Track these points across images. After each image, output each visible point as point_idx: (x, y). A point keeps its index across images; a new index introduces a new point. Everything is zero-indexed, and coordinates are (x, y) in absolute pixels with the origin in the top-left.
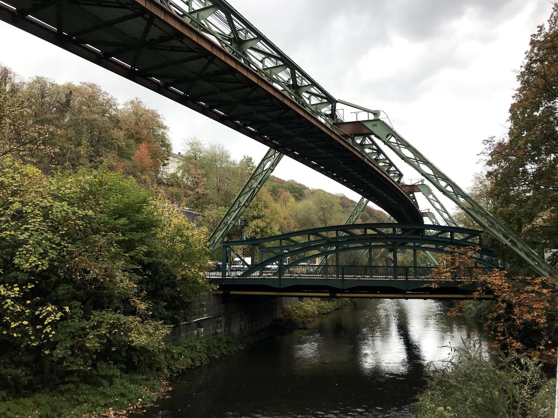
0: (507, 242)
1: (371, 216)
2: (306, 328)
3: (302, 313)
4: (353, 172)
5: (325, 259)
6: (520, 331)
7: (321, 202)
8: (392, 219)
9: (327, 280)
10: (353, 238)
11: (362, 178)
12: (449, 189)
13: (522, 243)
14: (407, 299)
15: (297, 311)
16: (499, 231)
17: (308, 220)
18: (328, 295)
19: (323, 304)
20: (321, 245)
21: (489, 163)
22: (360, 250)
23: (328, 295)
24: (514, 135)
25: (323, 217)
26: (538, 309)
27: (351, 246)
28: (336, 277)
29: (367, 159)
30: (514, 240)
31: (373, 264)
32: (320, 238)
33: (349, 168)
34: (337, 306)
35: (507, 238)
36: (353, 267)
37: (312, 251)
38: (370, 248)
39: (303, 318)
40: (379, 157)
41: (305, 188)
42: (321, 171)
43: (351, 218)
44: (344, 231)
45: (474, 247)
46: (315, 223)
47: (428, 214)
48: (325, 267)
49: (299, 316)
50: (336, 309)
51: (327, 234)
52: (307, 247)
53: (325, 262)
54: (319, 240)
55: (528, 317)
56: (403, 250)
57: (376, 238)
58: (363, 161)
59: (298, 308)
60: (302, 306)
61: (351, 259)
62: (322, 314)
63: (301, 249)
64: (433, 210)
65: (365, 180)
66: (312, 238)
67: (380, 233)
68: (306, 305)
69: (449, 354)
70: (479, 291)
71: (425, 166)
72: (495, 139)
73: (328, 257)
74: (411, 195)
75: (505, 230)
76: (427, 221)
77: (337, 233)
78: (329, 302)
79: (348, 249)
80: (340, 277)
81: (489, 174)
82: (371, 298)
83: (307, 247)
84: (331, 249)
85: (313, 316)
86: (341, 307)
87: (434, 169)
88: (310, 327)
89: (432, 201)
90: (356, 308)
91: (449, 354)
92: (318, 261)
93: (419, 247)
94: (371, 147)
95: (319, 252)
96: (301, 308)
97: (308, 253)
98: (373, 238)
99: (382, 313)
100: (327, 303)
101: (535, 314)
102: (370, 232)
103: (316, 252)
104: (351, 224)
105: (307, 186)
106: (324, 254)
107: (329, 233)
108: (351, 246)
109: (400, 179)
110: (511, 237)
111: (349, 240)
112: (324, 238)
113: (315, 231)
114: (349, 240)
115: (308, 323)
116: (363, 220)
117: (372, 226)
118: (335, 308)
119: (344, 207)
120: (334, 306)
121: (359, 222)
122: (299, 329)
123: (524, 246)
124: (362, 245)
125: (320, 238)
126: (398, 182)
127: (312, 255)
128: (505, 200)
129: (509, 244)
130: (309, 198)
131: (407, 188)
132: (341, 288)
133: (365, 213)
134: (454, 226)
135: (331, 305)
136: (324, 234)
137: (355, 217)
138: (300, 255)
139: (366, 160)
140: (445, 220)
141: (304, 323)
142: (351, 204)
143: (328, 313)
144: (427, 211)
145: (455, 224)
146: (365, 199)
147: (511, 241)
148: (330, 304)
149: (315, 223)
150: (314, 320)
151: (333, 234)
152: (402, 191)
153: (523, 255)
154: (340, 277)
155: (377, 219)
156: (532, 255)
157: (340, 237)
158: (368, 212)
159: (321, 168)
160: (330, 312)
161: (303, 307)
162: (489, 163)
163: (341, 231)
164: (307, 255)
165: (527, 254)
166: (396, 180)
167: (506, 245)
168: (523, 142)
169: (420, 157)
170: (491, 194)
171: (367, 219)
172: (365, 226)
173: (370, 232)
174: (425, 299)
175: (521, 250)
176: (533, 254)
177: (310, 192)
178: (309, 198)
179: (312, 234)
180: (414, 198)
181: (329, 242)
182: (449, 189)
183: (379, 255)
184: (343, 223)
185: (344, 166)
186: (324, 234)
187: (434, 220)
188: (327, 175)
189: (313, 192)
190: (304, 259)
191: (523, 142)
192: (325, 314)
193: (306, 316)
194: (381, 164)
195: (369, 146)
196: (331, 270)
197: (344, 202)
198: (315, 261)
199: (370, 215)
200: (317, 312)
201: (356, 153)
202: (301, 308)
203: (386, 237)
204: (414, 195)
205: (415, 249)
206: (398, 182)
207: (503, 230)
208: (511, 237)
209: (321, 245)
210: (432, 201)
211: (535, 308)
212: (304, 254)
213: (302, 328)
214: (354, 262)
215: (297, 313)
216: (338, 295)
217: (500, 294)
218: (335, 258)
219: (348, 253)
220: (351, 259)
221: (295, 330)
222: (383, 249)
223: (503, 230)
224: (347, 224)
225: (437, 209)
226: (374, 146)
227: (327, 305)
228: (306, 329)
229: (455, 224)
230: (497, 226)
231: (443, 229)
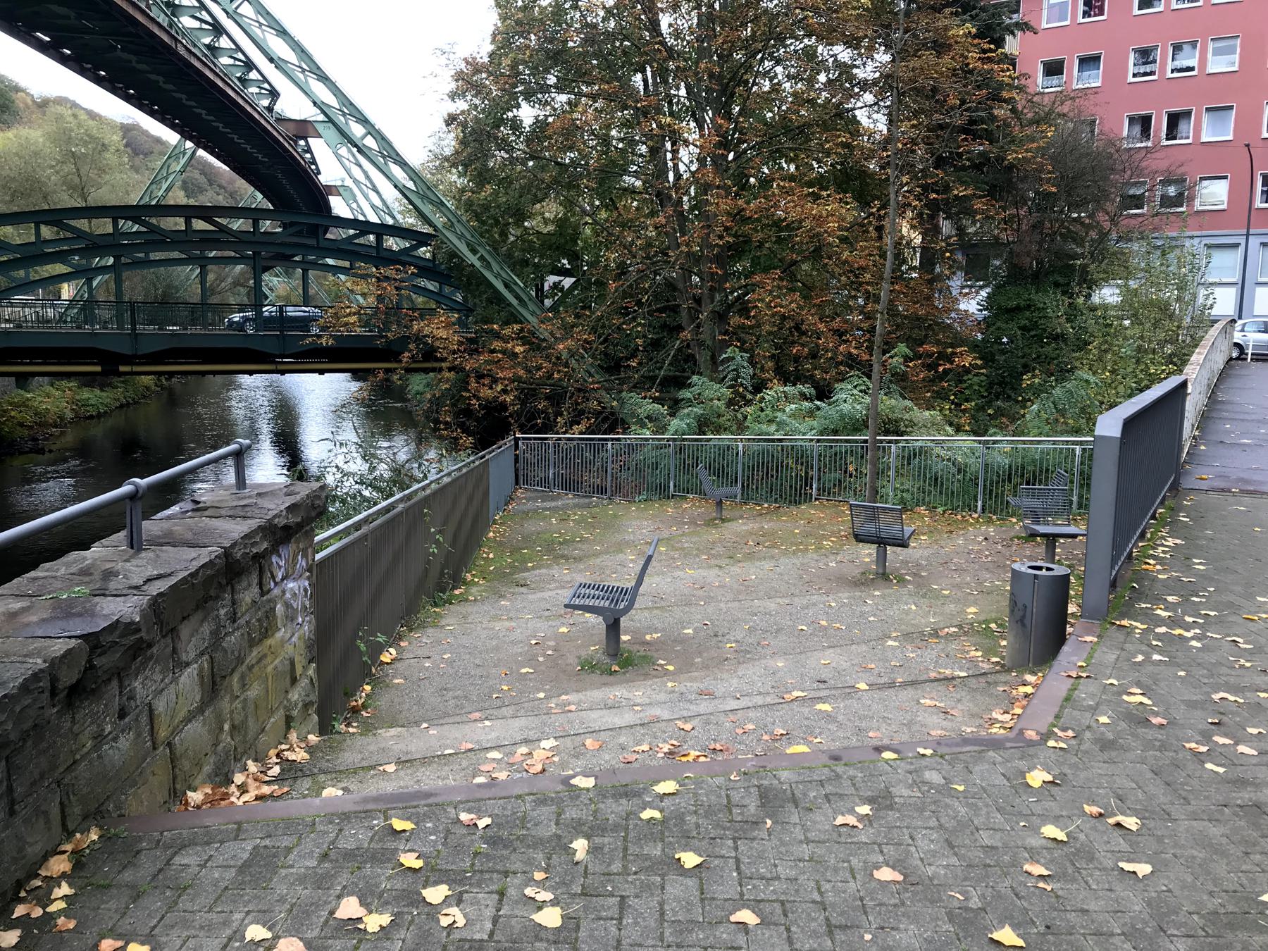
0: (472, 259)
1: (211, 182)
2: (43, 449)
3: (28, 418)
4: (150, 73)
5: (85, 288)
6: (478, 420)
7: (64, 137)
8: (259, 196)
9: (93, 335)
10: (159, 239)
11: (174, 91)
12: (370, 142)
13: (499, 263)
14: (283, 373)
15: (13, 413)
16: (461, 237)
17: (31, 184)
18: (98, 369)
19: (86, 394)
20: (73, 252)
21: (453, 96)
22: (180, 268)
23: (98, 369)
24: (503, 41)
25: (77, 180)
26: (504, 379)
27: (155, 256)
28: (118, 329)
29: (185, 47)
30: (487, 257)
31: (215, 300)
32: (69, 235)
33: (138, 62)
34: (125, 398)
35: (474, 252)
36: (164, 306)
37: (49, 267)
38: (203, 263)
39: (31, 427)
40: (218, 40)
41: (17, 89)
42: (64, 60)
43: (154, 186)
44: (136, 220)
45: (404, 267)
46: (55, 192)
47: (341, 190)
48: (87, 306)
49: (21, 425)
50: (122, 406)
51: (90, 223)
52: (33, 255)
53: (86, 295)
54: (66, 239)
55: (486, 393)
56: (291, 270)
57: (218, 241)
58: (176, 53)
59: (15, 405)
60: (28, 399)
61: (156, 289)
62: (83, 418)
63: (16, 260)
64: (349, 182)
65: (184, 96)
66: (47, 232)
67: (223, 229)
68: (41, 399)
69: (330, 451)
70: (411, 351)
71: (321, 84)
72: (456, 49)
73: (95, 284)
74: (302, 143)
75: (472, 236)
76: (339, 207)
77: (115, 224)
78: (102, 390)
79: (148, 263)
80: (128, 329)
81: (451, 120)
82: (203, 373)
83: (33, 255)
84: (103, 263)
85: (61, 422)
86: (134, 399)
87: (341, 97)
88: (54, 448)
89: (346, 162)
90: (172, 400)
91: (330, 451)
92: (67, 291)
93: (315, 265)
94: (198, 15)
95: (70, 270)
96: (27, 406)
97: (36, 272)
98: (207, 240)
99: (238, 411)
100: (97, 392)
101: (499, 388)
102: (199, 225)
103: (60, 268)
104: (154, 203)
105: (23, 84)
106: (86, 274)
107: (94, 221)
108: (155, 256)
109: (274, 102)
110: (482, 251)
111: (147, 243)
112: (80, 235)
113: (56, 217)
114: (147, 243)
115: (46, 439)
116: (187, 187)
117: (205, 213)
118: (117, 404)
119: (137, 154)
120: (118, 400)
121: (179, 197)
122: (22, 453)
123: (502, 268)
124: (233, 254)
125: (69, 235)
126: (270, 109)
127: (47, 275)
128: (480, 174)
129: (478, 264)
130: (30, 121)
131: (291, 125)
132: (129, 353)
133: (196, 174)
134: (390, 221)
135: (108, 397)
136: (82, 224)
137: (165, 186)
138: (15, 274)
139: (182, 52)
140: (373, 207)
141: (35, 440)
142: (158, 148)
143: (99, 416)
144: (339, 183)
145: (393, 217)
146: (189, 144)
147: (482, 258)
148: (104, 394)
149: (55, 192)
150: (63, 433)
151: (104, 226)
152: (275, 133)
153: (499, 286)
154: (128, 329)
155: (226, 191)
156: (514, 287)
157: (123, 234)
158: (203, 173)
159: (63, 54)
160: (106, 412)
161: (30, 403)
162: (453, 96)
163: (127, 219)
164: (33, 276)
165: (506, 286)
166: (265, 103)
167: (473, 265)
168: (509, 63)
169: (312, 65)
170: (452, 162)
171: (202, 190)
172: (188, 212)
173: (199, 225)
174: (322, 372)
175: (497, 276)
176: (516, 284)
177: (34, 101)
178: (30, 121)
179: (47, 223)
180: (309, 151)
181: (96, 245)
182: (370, 142)
183: (230, 280)
184: (133, 200)
185: (125, 56)
186: (82, 224)
187: (354, 206)
188: (82, 72)
189: (44, 104)
190: (27, 286)
191: (509, 63)
192: (91, 417)
193: (40, 424)
194: (225, 60)
195: (192, 12)
196: (104, 313)
197: (131, 137)
198: (59, 292)
199: (209, 180)
200: (69, 415)
201: (156, 31)
202: (24, 404)
203: (240, 240)
204: (307, 144)
205: (306, 266)
206: (270, 109)
207: (469, 237)
208: (482, 251)
209: (73, 252)
210: (346, 162)
211: (501, 378)
212: (27, 274)
213: (31, 451)
214: (165, 294)
215: (13, 417)
216: (122, 369)
217: (445, 355)
218: (112, 285)
219: (149, 273)
220: (156, 289)
221: (12, 455)
222: (239, 268)
223: (469, 237)
224: (141, 204)
225: (356, 181)
226: (204, 13)
227: (95, 397)
228: (41, 451)
229: (393, 217)
230: (459, 228)
231: (364, 227)
